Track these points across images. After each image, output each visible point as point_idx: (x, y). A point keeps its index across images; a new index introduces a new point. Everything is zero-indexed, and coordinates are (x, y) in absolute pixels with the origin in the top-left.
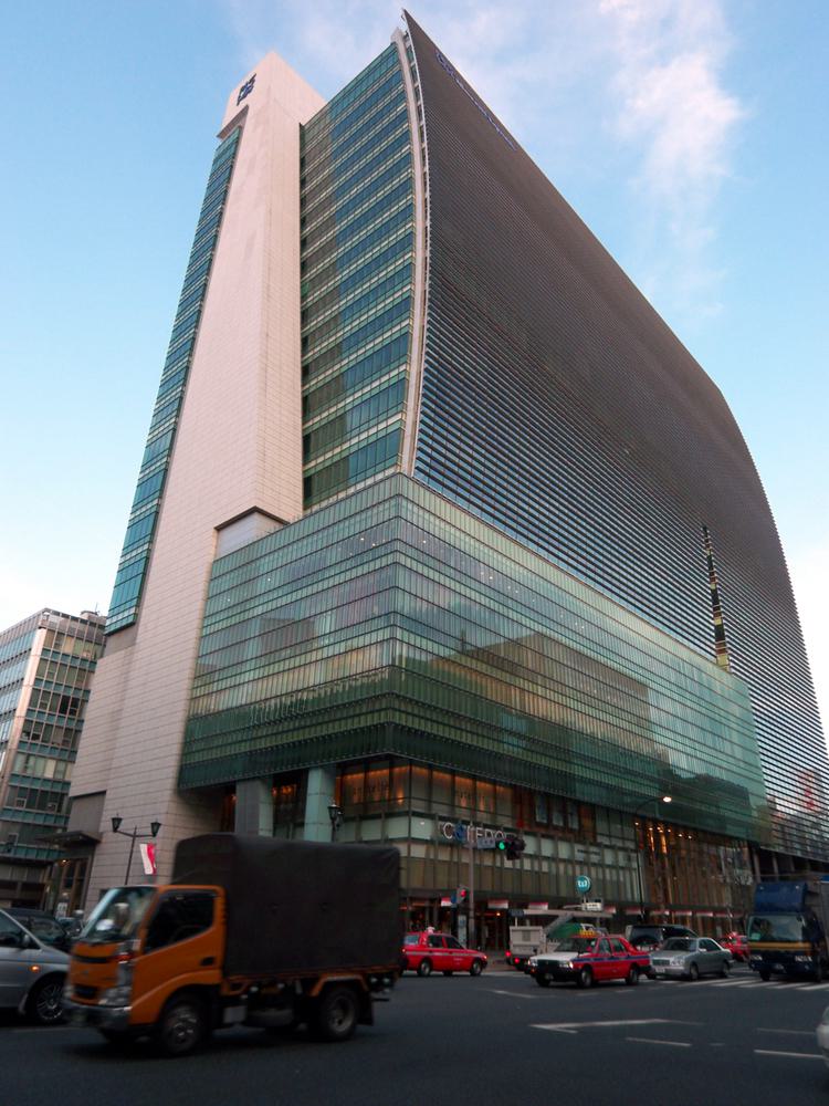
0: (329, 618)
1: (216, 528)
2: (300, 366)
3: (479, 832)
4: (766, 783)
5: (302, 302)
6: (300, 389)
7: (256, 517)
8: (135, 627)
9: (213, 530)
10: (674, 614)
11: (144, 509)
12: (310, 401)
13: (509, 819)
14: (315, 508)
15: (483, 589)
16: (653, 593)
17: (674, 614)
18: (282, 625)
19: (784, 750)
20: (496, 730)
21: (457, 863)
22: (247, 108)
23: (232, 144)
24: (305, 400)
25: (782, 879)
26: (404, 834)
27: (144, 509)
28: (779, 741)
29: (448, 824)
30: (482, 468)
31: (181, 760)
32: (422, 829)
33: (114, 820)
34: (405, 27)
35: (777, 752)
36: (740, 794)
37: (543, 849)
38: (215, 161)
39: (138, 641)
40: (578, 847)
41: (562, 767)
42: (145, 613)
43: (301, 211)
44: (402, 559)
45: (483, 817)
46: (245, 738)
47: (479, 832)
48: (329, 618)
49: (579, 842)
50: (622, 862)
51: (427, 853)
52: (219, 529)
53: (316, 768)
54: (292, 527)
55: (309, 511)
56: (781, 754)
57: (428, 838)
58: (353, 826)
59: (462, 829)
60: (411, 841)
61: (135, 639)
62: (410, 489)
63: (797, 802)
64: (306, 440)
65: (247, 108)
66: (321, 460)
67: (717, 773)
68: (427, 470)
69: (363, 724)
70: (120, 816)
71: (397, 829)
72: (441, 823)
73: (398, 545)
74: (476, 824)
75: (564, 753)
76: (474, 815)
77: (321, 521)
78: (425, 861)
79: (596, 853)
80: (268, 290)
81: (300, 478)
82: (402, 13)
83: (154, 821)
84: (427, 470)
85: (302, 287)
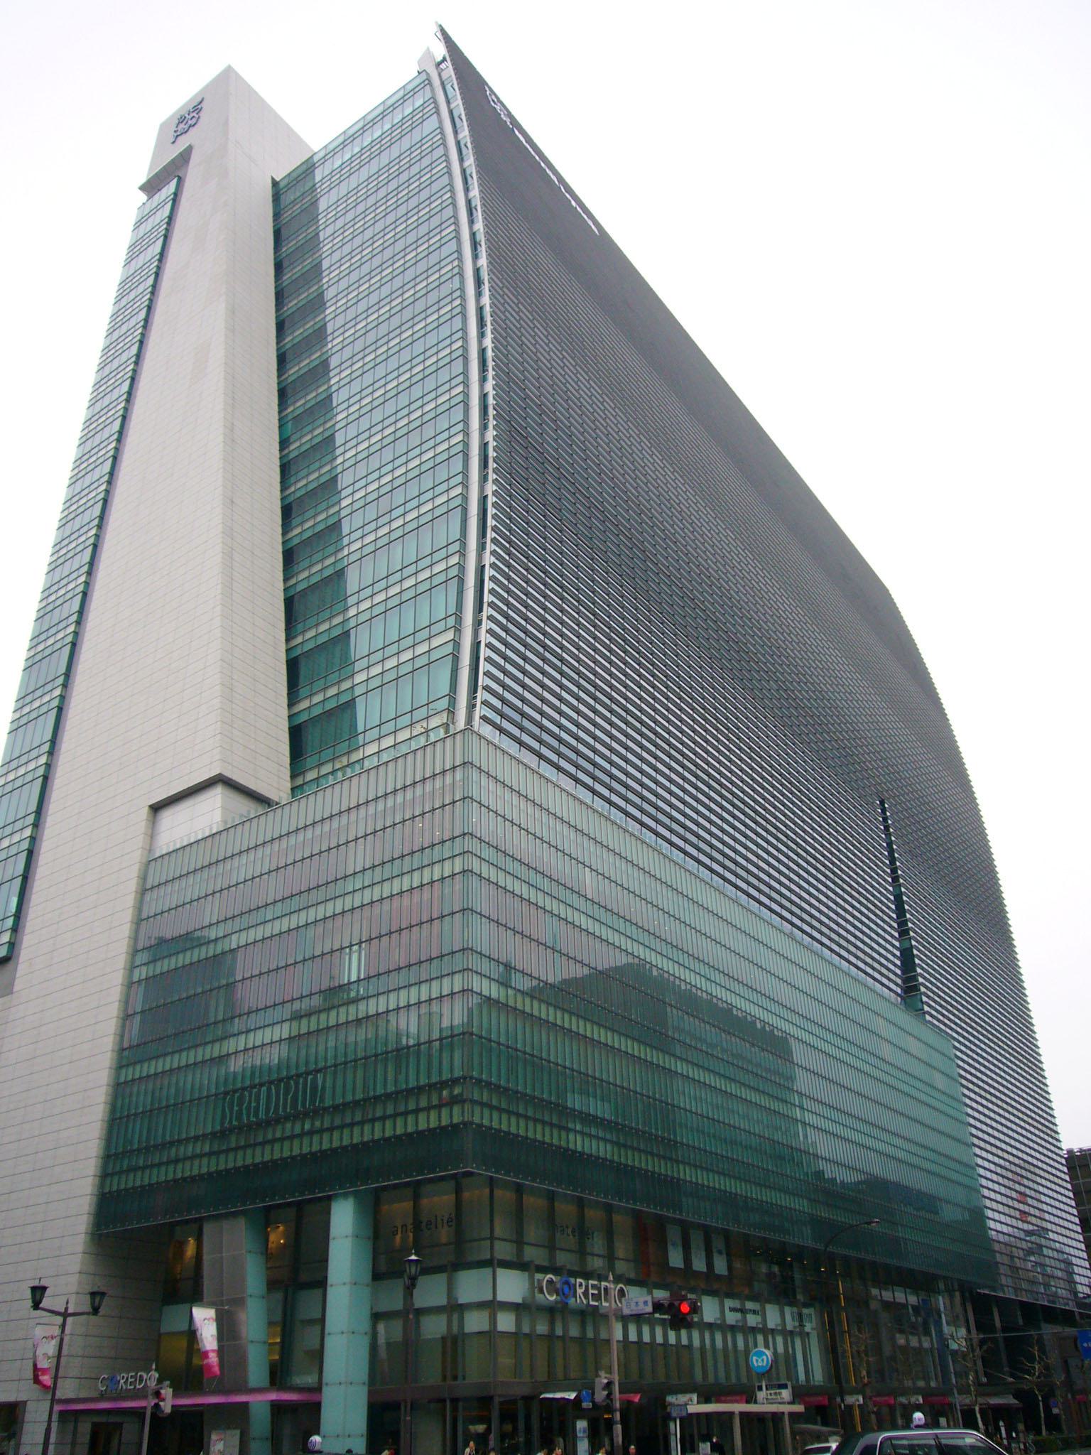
0: (355, 957)
1: (151, 807)
2: (280, 549)
3: (594, 1287)
4: (986, 1192)
5: (281, 450)
6: (281, 586)
7: (218, 792)
8: (10, 965)
9: (146, 810)
10: (787, 893)
11: (22, 771)
12: (298, 606)
13: (632, 1265)
14: (311, 775)
15: (589, 908)
16: (782, 868)
17: (803, 894)
18: (195, 944)
19: (1016, 1136)
20: (562, 1115)
21: (562, 1338)
22: (189, 150)
23: (165, 202)
24: (289, 603)
25: (444, 1401)
26: (442, 1300)
27: (22, 771)
28: (992, 1115)
29: (550, 1276)
30: (694, 792)
31: (102, 1185)
32: (512, 1286)
33: (34, 1289)
34: (440, 51)
35: (1002, 1137)
36: (927, 1203)
37: (182, 1329)
38: (139, 224)
39: (16, 988)
40: (729, 1303)
41: (663, 1168)
42: (29, 941)
43: (277, 310)
44: (476, 865)
45: (597, 1263)
46: (198, 1151)
47: (594, 1287)
48: (355, 957)
49: (730, 1295)
50: (790, 1324)
51: (518, 1323)
52: (156, 808)
53: (345, 1196)
54: (287, 809)
55: (299, 781)
56: (1013, 1142)
57: (520, 1301)
58: (441, 1278)
59: (567, 1283)
60: (493, 1306)
61: (12, 984)
62: (481, 755)
63: (1007, 1210)
64: (293, 666)
65: (189, 150)
66: (318, 698)
67: (891, 1173)
68: (497, 719)
69: (422, 1126)
70: (43, 1283)
71: (471, 1286)
72: (538, 1276)
73: (468, 844)
74: (587, 1276)
75: (668, 1147)
76: (611, 1268)
77: (336, 802)
78: (516, 1335)
79: (754, 1312)
80: (232, 430)
81: (285, 726)
82: (436, 29)
83: (36, 1283)
84: (497, 719)
85: (281, 426)
